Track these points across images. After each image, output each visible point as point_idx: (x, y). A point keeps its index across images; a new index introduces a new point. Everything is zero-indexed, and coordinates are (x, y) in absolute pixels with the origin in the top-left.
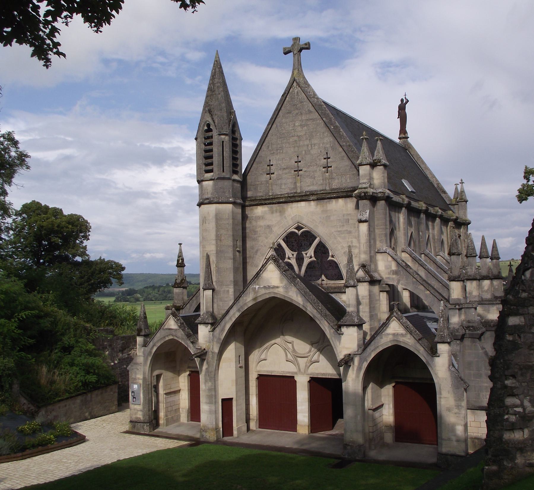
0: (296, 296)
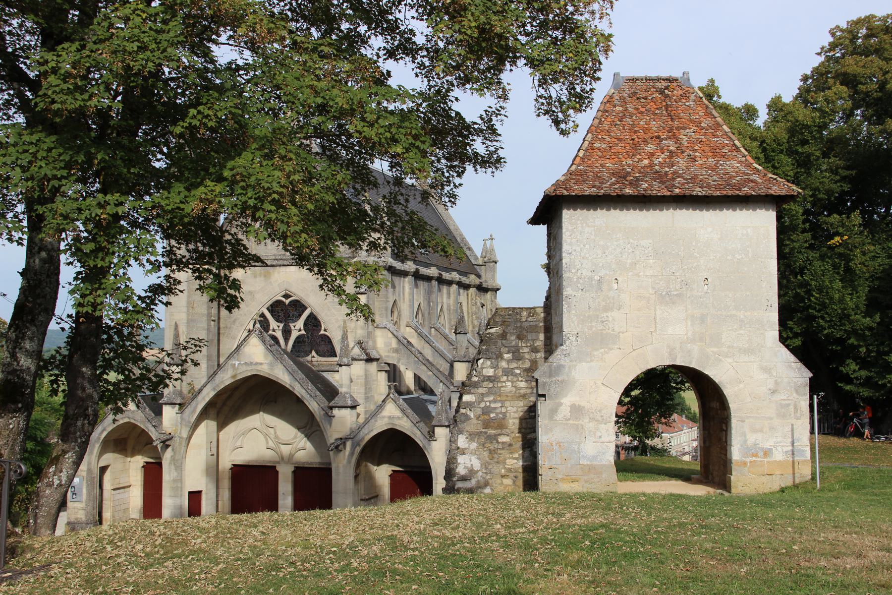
0: (282, 375)
